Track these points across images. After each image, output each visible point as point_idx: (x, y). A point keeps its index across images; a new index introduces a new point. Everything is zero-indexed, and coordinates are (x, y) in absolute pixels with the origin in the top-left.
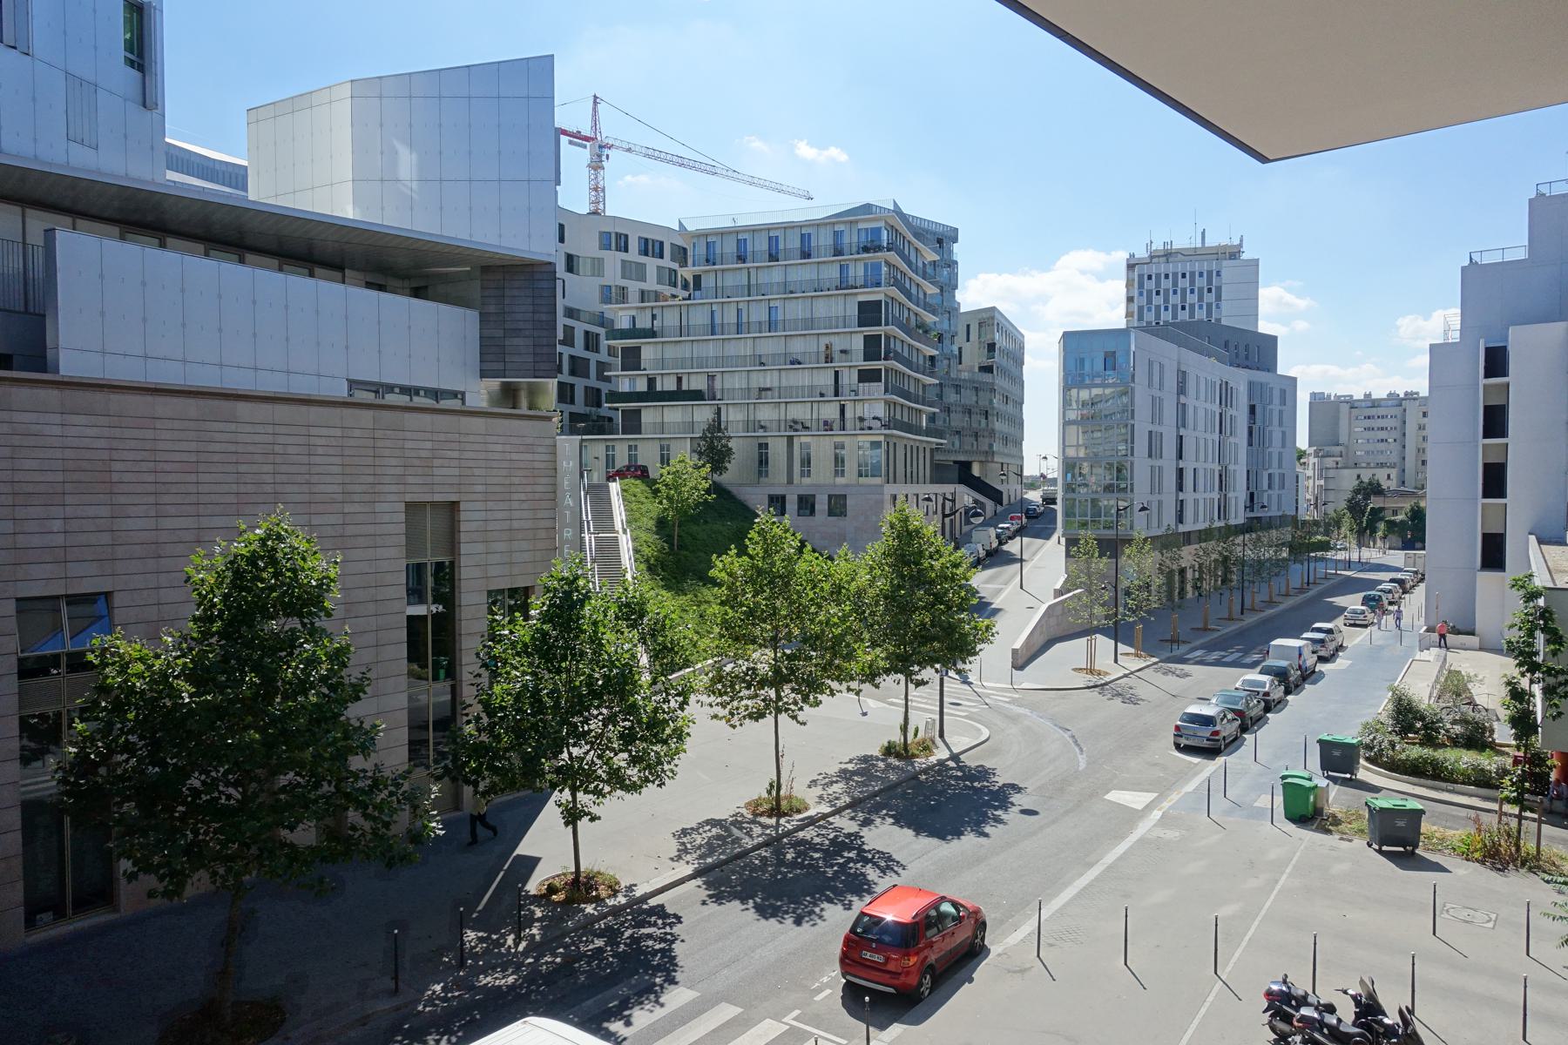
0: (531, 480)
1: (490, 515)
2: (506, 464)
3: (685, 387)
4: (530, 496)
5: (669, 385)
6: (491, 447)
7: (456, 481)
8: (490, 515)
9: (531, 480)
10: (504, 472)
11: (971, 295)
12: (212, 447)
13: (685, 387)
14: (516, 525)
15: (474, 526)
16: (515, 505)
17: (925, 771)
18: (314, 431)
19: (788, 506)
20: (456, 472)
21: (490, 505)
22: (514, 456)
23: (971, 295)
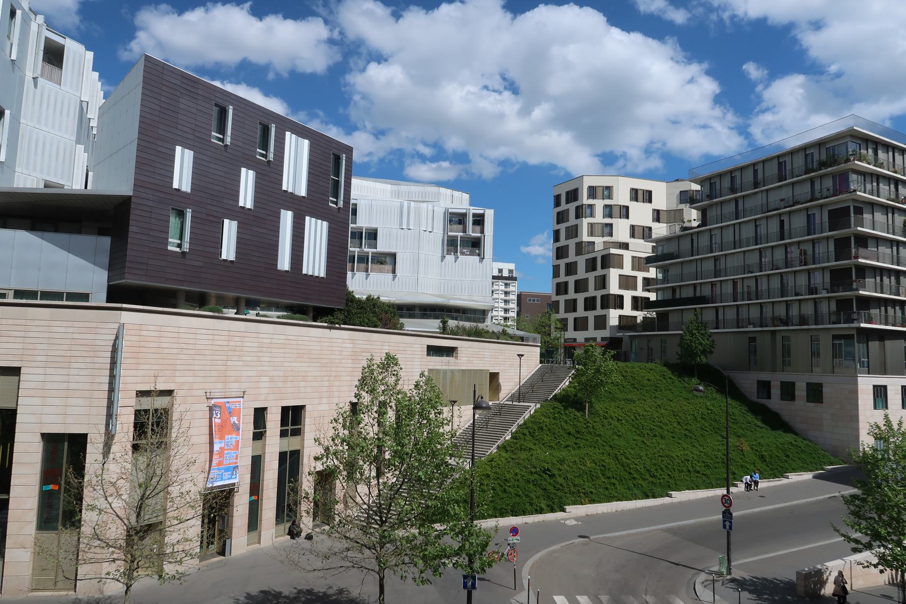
0: (91, 354)
1: (48, 378)
2: (67, 342)
3: (678, 296)
4: (91, 366)
5: (688, 293)
6: (199, 337)
7: (20, 352)
8: (48, 378)
9: (91, 354)
10: (66, 347)
11: (97, 74)
12: (31, 334)
13: (678, 296)
14: (73, 386)
15: (32, 385)
16: (73, 372)
17: (867, 534)
18: (164, 329)
19: (772, 391)
20: (20, 346)
21: (49, 371)
22: (75, 336)
23: (97, 74)
